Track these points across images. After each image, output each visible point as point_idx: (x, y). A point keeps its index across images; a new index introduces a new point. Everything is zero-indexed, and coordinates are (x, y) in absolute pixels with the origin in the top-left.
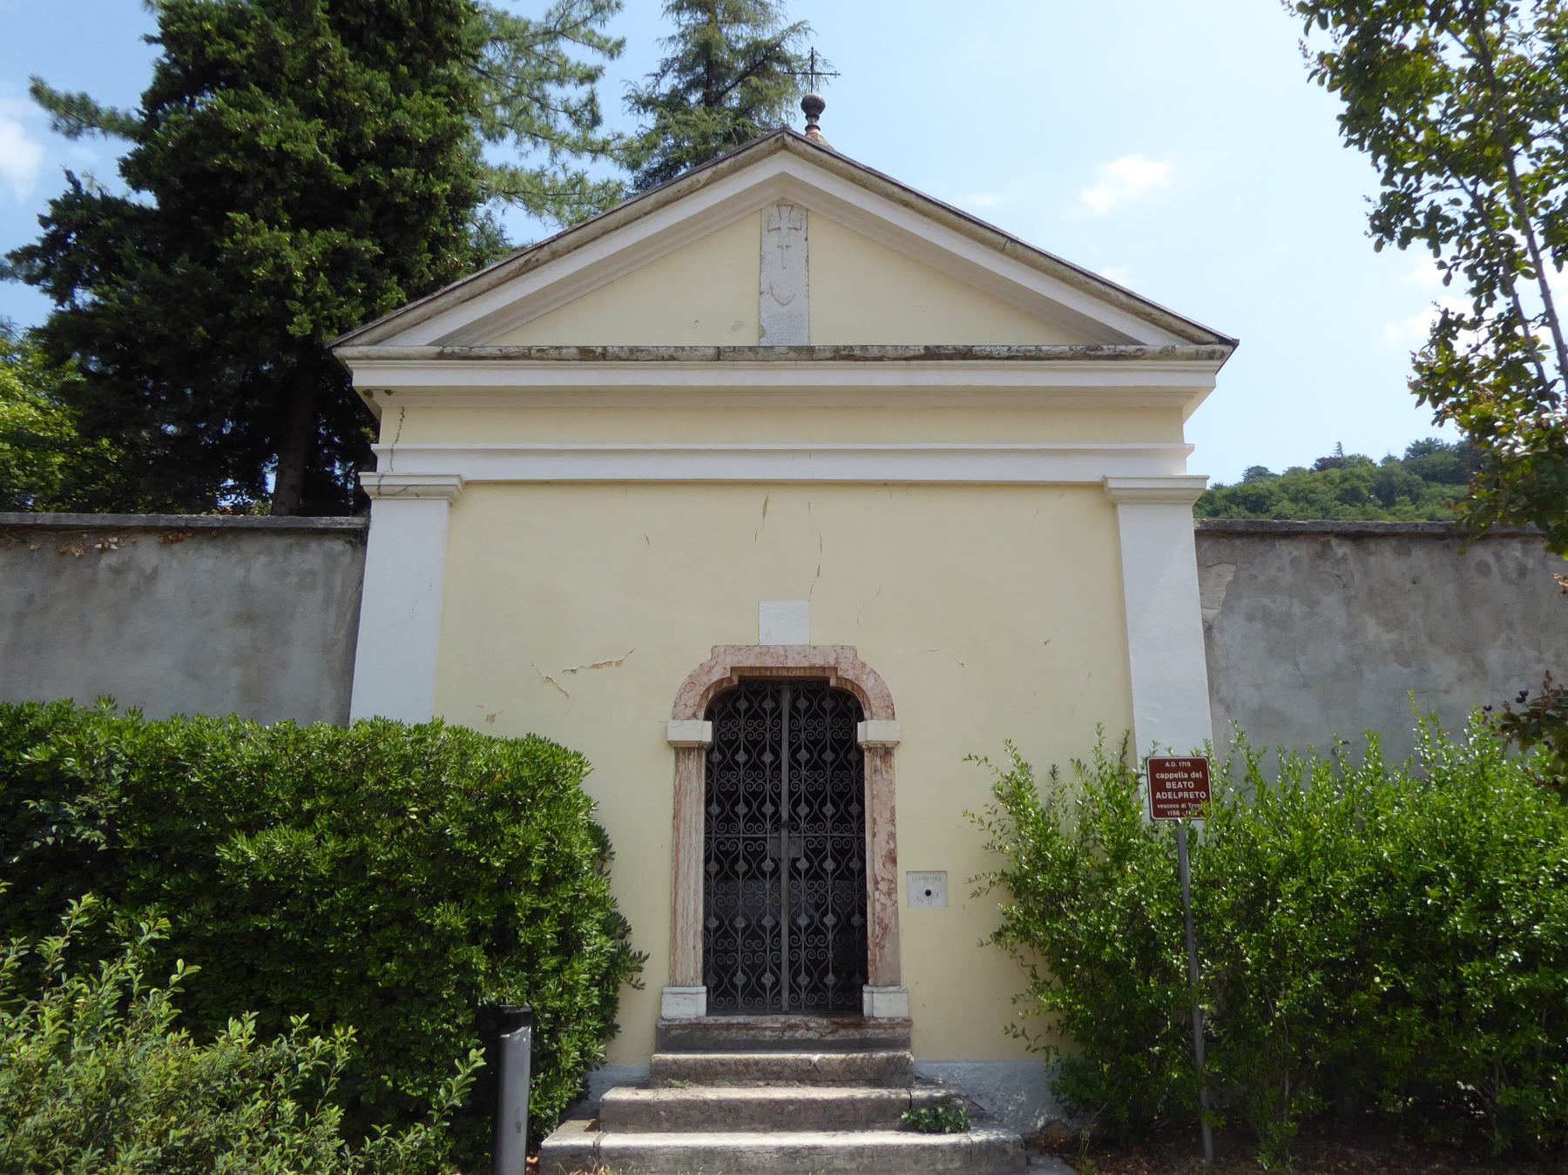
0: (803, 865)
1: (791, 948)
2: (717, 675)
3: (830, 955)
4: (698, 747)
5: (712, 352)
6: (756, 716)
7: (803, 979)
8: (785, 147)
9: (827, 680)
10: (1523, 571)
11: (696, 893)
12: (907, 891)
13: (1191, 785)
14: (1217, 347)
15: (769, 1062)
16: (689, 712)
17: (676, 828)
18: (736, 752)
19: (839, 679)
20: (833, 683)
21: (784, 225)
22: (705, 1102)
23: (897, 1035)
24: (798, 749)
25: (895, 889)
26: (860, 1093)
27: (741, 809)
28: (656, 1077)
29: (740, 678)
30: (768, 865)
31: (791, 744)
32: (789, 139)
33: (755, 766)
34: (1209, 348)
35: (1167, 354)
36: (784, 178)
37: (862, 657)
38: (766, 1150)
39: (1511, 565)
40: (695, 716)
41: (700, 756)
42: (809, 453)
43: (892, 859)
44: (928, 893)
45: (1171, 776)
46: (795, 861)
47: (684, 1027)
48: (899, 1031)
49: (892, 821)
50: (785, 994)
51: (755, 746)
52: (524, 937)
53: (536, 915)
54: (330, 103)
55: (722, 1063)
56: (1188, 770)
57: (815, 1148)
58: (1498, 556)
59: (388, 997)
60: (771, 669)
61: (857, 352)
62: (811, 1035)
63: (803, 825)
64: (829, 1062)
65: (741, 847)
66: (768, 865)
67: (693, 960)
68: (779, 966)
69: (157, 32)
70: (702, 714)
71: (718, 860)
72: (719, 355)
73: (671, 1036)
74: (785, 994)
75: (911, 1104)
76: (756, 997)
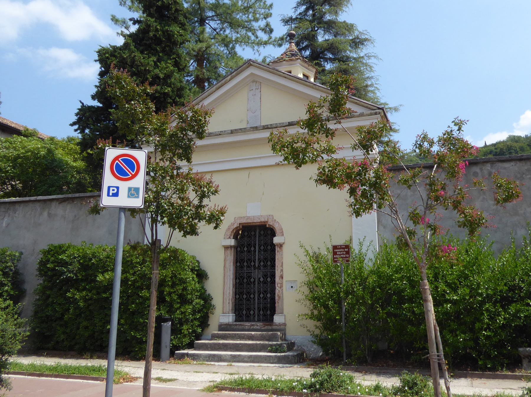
0: (262, 279)
1: (258, 303)
2: (235, 226)
3: (269, 305)
4: (231, 247)
5: (230, 131)
6: (250, 237)
7: (261, 312)
8: (251, 65)
9: (266, 225)
10: (490, 174)
11: (229, 288)
12: (286, 286)
13: (344, 253)
14: (377, 111)
15: (241, 334)
16: (228, 237)
17: (224, 270)
18: (244, 247)
19: (269, 225)
20: (267, 226)
21: (254, 88)
22: (219, 343)
23: (282, 328)
24: (261, 246)
25: (282, 286)
26: (258, 342)
27: (245, 264)
28: (214, 337)
29: (243, 226)
30: (252, 280)
31: (259, 245)
32: (251, 63)
33: (249, 251)
34: (375, 111)
35: (362, 115)
36: (252, 74)
37: (275, 218)
38: (228, 355)
39: (486, 172)
40: (230, 238)
41: (231, 249)
42: (260, 158)
43: (282, 277)
44: (292, 287)
45: (339, 250)
46: (260, 278)
47: (225, 325)
48: (282, 327)
49: (282, 266)
50: (256, 316)
51: (249, 246)
52: (168, 299)
53: (170, 294)
54: (138, 71)
55: (229, 334)
56: (344, 248)
57: (240, 355)
58: (481, 170)
59: (133, 313)
60: (250, 223)
61: (269, 126)
62: (258, 327)
63: (262, 268)
64: (257, 334)
65: (245, 274)
66: (252, 280)
67: (229, 306)
68: (255, 309)
69: (97, 58)
70: (232, 237)
71: (239, 279)
72: (232, 132)
73: (223, 327)
74: (256, 316)
75: (271, 346)
76: (248, 319)
